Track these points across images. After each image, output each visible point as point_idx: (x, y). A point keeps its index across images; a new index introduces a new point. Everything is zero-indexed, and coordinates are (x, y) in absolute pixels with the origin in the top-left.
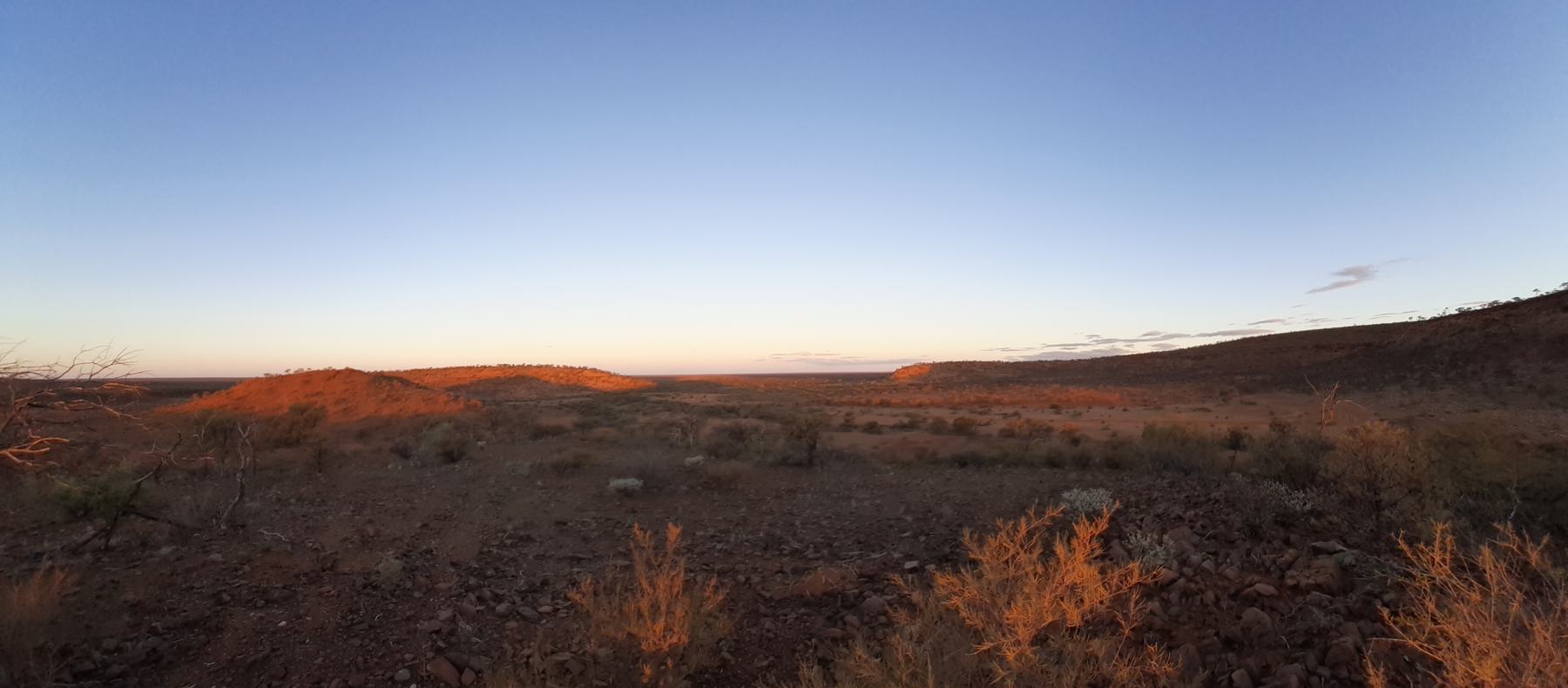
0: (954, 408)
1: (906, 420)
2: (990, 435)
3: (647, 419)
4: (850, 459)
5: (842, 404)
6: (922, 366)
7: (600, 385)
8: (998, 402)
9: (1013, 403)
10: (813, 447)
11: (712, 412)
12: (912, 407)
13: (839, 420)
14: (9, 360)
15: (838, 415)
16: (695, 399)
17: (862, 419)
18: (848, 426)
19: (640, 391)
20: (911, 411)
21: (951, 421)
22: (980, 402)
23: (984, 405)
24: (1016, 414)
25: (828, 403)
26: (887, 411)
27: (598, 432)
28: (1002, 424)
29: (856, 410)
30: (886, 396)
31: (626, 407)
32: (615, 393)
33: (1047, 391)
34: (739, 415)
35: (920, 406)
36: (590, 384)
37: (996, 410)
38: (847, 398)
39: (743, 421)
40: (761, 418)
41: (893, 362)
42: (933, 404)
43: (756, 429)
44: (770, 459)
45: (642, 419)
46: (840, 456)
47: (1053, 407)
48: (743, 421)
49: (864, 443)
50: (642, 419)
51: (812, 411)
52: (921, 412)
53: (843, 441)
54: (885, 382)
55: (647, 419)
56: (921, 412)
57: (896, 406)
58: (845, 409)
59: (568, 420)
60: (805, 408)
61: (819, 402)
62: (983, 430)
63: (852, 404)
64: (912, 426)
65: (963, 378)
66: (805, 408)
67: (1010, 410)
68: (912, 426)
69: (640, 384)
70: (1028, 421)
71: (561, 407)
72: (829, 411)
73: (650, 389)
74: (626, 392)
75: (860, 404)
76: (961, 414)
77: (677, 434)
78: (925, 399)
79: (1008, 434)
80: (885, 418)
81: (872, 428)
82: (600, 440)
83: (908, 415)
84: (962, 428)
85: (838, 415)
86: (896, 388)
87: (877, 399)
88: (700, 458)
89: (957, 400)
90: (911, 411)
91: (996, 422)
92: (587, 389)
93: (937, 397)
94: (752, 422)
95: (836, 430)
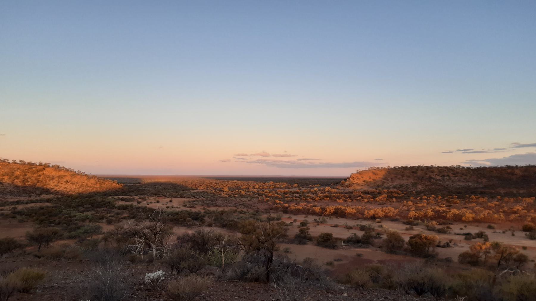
0: (410, 223)
1: (360, 234)
2: (448, 260)
3: (111, 228)
4: (305, 274)
5: (297, 212)
6: (375, 171)
7: (63, 187)
8: (458, 219)
9: (476, 221)
10: (270, 260)
11: (177, 219)
12: (366, 219)
13: (294, 231)
14: (3, 158)
15: (293, 223)
16: (160, 204)
17: (316, 231)
18: (303, 238)
19: (106, 194)
20: (365, 223)
21: (407, 239)
22: (439, 216)
23: (444, 221)
24: (480, 235)
25: (286, 211)
26: (341, 221)
27: (57, 245)
28: (464, 247)
29: (311, 219)
30: (340, 205)
31: (89, 214)
32: (80, 196)
33: (518, 207)
34: (203, 222)
35: (373, 218)
36: (52, 185)
37: (456, 228)
38: (302, 206)
39: (207, 230)
40: (224, 226)
41: (313, 166)
42: (387, 217)
43: (218, 239)
44: (229, 273)
45: (106, 228)
46: (295, 270)
47: (526, 229)
48: (207, 230)
49: (321, 257)
50: (106, 228)
51: (269, 219)
52: (375, 225)
53: (300, 254)
54: (340, 189)
55: (111, 228)
56: (375, 225)
57: (354, 217)
58: (301, 218)
59: (20, 233)
60: (264, 216)
61: (276, 209)
62: (442, 252)
63: (308, 212)
64: (365, 242)
65: (420, 187)
66: (264, 216)
67: (474, 230)
68: (365, 242)
69: (108, 185)
70: (496, 246)
71: (15, 214)
72: (286, 219)
73: (115, 192)
74: (91, 195)
75: (314, 213)
76: (417, 230)
77: (140, 245)
78: (379, 211)
79: (471, 260)
80: (340, 229)
81: (326, 241)
82: (57, 256)
83: (362, 228)
84: (419, 248)
85: (293, 223)
86: (351, 196)
87: (331, 208)
88: (160, 273)
89: (412, 214)
90: (365, 223)
91: (456, 243)
92: (47, 191)
93: (391, 209)
94: (217, 231)
95: (292, 242)
